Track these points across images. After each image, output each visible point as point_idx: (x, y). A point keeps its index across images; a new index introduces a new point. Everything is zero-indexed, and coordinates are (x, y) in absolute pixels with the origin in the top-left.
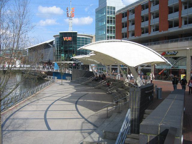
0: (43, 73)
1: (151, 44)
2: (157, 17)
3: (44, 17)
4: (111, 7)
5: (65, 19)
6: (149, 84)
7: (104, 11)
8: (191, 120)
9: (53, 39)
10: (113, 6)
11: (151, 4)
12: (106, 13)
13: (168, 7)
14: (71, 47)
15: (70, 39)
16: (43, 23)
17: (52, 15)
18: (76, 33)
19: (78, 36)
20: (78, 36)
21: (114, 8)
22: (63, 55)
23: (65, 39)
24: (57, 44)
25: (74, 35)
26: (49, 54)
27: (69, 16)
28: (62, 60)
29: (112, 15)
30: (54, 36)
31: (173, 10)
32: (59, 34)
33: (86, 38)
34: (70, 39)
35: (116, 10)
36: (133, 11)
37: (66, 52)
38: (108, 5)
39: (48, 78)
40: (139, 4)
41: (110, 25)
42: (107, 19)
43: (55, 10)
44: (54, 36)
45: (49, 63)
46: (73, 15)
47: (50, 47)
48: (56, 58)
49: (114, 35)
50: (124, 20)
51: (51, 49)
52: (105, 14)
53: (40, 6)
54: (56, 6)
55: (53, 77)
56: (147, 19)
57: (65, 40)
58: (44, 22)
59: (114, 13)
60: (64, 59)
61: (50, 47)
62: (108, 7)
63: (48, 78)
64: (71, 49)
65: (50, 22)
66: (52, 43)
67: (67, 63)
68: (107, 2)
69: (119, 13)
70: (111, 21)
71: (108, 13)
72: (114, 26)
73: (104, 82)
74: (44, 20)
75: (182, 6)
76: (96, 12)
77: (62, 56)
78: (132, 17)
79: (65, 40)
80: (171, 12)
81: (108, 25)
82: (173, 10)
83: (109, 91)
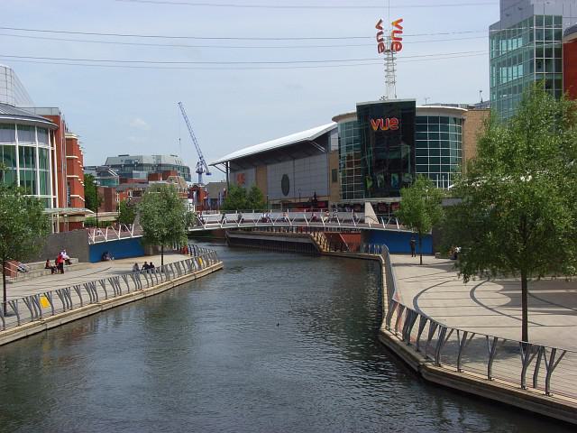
4: (549, 20)
20: (418, 114)
21: (559, 20)
27: (388, 47)
32: (355, 110)
34: (392, 124)
57: (375, 128)
66: (323, 139)
76: (492, 37)
79: (375, 128)
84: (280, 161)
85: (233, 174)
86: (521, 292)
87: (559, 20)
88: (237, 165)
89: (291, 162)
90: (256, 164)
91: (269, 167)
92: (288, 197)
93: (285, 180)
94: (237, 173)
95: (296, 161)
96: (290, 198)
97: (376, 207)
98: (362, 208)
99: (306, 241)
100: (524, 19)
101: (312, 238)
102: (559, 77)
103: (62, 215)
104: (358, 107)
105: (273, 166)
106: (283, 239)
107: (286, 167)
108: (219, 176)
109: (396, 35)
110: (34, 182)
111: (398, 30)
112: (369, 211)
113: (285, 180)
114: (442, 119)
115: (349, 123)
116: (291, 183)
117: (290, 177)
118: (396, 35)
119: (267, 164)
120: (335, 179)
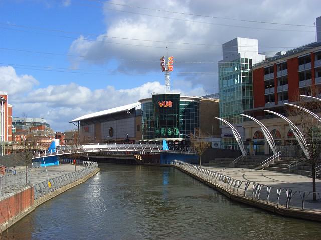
1: (263, 119)
2: (285, 83)
4: (247, 60)
8: (172, 238)
10: (249, 58)
11: (314, 57)
13: (300, 73)
15: (169, 104)
18: (179, 95)
19: (180, 100)
21: (251, 60)
23: (161, 104)
25: (175, 98)
30: (141, 101)
31: (305, 76)
32: (151, 97)
34: (169, 104)
35: (253, 64)
36: (284, 66)
38: (242, 57)
40: (294, 57)
44: (141, 101)
50: (269, 77)
54: (14, 68)
56: (273, 84)
62: (243, 59)
71: (243, 68)
75: (277, 83)
76: (219, 66)
78: (284, 73)
80: (302, 79)
82: (305, 76)
84: (108, 121)
85: (82, 127)
86: (141, 166)
87: (251, 60)
89: (115, 122)
90: (95, 122)
91: (102, 124)
92: (113, 138)
93: (111, 130)
94: (84, 127)
95: (118, 121)
96: (114, 138)
97: (167, 143)
98: (160, 143)
99: (132, 159)
100: (236, 59)
101: (135, 157)
102: (251, 85)
103: (6, 145)
104: (153, 96)
105: (105, 123)
106: (118, 158)
107: (113, 124)
108: (74, 128)
110: (147, 103)
112: (164, 144)
113: (111, 130)
115: (148, 103)
116: (115, 131)
117: (114, 129)
119: (101, 122)
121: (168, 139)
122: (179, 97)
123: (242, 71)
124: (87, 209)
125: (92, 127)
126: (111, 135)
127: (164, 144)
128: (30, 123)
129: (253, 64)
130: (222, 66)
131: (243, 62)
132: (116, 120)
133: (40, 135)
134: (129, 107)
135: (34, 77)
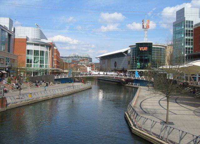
0: (124, 80)
2: (28, 51)
3: (105, 23)
4: (189, 21)
5: (127, 25)
6: (139, 83)
7: (183, 25)
9: (128, 49)
12: (184, 27)
14: (147, 56)
15: (145, 49)
16: (104, 29)
17: (114, 21)
18: (152, 43)
19: (153, 46)
20: (153, 46)
21: (192, 22)
22: (139, 64)
24: (133, 53)
25: (149, 45)
26: (123, 63)
27: (145, 27)
28: (138, 69)
29: (190, 28)
32: (135, 44)
33: (161, 48)
34: (145, 49)
37: (141, 61)
38: (186, 19)
39: (130, 84)
41: (188, 38)
42: (185, 32)
43: (117, 16)
44: (130, 46)
45: (124, 71)
46: (148, 26)
47: (124, 56)
48: (131, 66)
49: (192, 47)
51: (125, 57)
52: (183, 27)
53: (134, 22)
55: (131, 84)
57: (141, 50)
58: (105, 28)
59: (192, 26)
60: (139, 67)
61: (124, 56)
62: (187, 21)
63: (129, 84)
64: (146, 58)
65: (111, 27)
66: (126, 52)
67: (142, 72)
68: (185, 16)
69: (197, 26)
70: (189, 33)
72: (192, 38)
73: (188, 89)
74: (106, 26)
76: (174, 26)
77: (138, 65)
79: (141, 50)
81: (186, 38)
83: (197, 96)
84: (114, 58)
87: (192, 22)
88: (103, 58)
95: (119, 58)
105: (113, 59)
107: (116, 60)
109: (148, 24)
111: (148, 22)
112: (137, 73)
114: (161, 50)
116: (117, 64)
118: (148, 24)
120: (129, 64)
121: (140, 70)
122: (152, 45)
123: (186, 29)
124: (56, 80)
125: (106, 60)
126: (115, 66)
127: (137, 73)
128: (81, 57)
129: (194, 24)
130: (176, 25)
131: (187, 22)
132: (118, 57)
133: (81, 64)
134: (123, 51)
135: (71, 38)
